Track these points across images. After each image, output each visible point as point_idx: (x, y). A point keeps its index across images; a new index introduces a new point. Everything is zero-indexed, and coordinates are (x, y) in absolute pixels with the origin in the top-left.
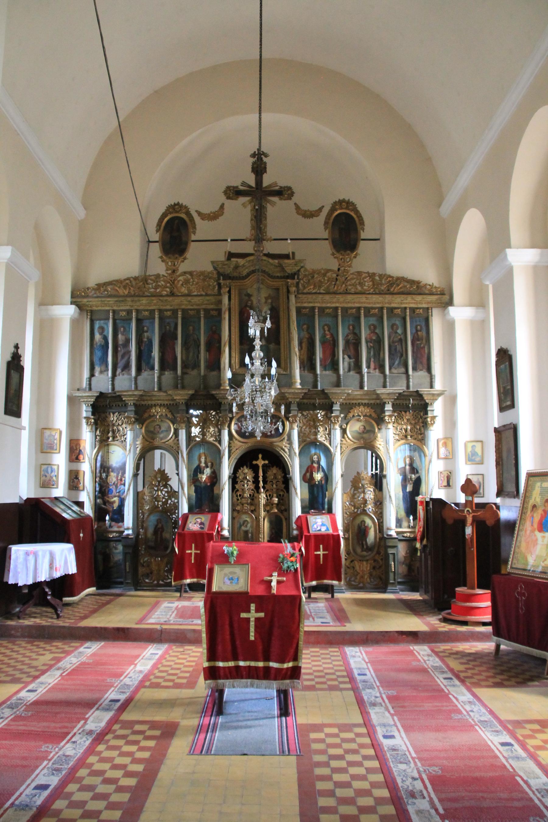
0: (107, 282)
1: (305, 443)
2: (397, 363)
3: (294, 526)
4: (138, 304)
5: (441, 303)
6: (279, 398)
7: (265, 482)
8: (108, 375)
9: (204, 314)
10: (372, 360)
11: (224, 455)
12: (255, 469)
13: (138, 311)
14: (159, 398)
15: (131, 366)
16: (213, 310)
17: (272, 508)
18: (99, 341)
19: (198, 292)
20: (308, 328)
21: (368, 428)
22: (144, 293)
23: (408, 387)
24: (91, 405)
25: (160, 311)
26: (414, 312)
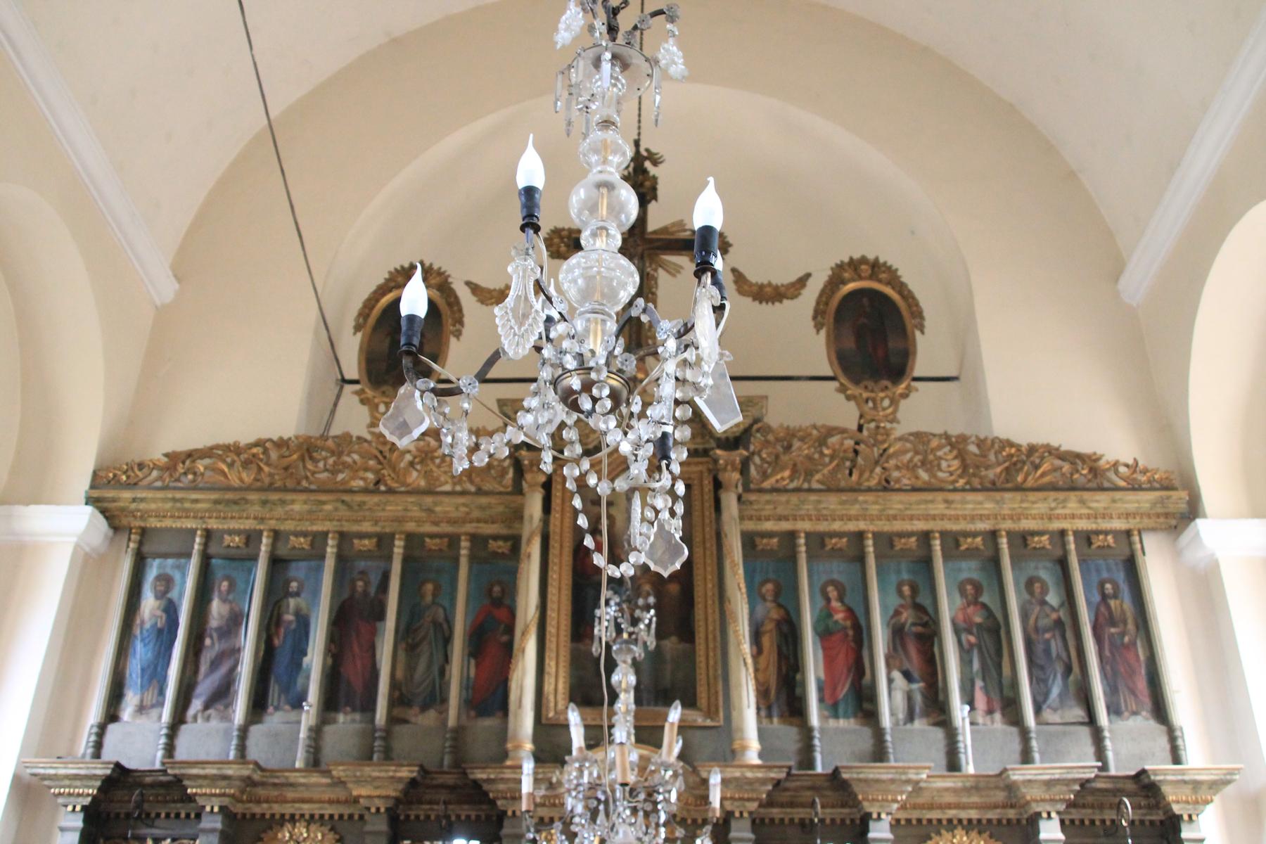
0: (196, 450)
2: (1055, 691)
4: (279, 511)
5: (1167, 515)
6: (691, 800)
8: (160, 717)
9: (471, 549)
10: (979, 684)
13: (276, 535)
14: (306, 795)
15: (236, 692)
16: (496, 538)
18: (153, 616)
19: (454, 484)
20: (777, 594)
22: (299, 483)
24: (84, 808)
25: (343, 537)
26: (1090, 543)
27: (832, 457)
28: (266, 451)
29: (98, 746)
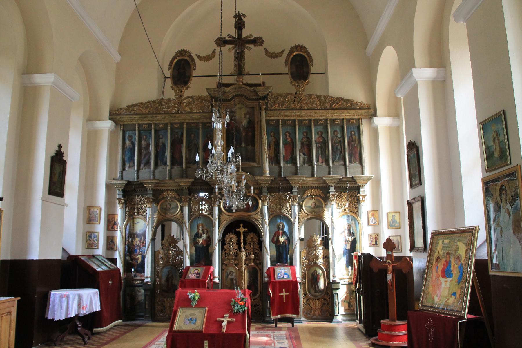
1: (273, 216)
2: (337, 158)
3: (266, 275)
4: (155, 119)
7: (245, 244)
10: (320, 156)
11: (215, 224)
12: (238, 234)
13: (156, 124)
17: (250, 263)
20: (275, 134)
21: (317, 204)
23: (346, 175)
27: (288, 101)
28: (150, 104)
29: (122, 176)
